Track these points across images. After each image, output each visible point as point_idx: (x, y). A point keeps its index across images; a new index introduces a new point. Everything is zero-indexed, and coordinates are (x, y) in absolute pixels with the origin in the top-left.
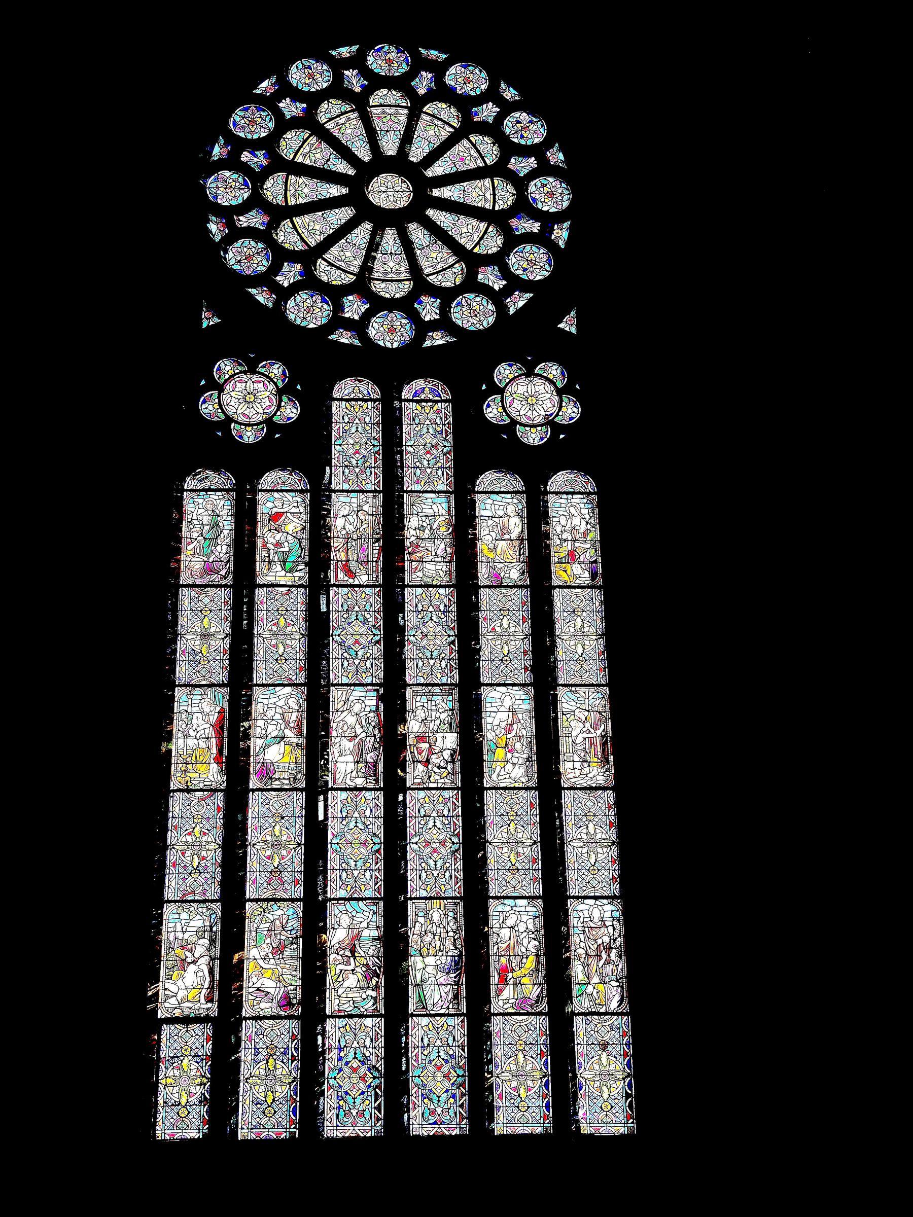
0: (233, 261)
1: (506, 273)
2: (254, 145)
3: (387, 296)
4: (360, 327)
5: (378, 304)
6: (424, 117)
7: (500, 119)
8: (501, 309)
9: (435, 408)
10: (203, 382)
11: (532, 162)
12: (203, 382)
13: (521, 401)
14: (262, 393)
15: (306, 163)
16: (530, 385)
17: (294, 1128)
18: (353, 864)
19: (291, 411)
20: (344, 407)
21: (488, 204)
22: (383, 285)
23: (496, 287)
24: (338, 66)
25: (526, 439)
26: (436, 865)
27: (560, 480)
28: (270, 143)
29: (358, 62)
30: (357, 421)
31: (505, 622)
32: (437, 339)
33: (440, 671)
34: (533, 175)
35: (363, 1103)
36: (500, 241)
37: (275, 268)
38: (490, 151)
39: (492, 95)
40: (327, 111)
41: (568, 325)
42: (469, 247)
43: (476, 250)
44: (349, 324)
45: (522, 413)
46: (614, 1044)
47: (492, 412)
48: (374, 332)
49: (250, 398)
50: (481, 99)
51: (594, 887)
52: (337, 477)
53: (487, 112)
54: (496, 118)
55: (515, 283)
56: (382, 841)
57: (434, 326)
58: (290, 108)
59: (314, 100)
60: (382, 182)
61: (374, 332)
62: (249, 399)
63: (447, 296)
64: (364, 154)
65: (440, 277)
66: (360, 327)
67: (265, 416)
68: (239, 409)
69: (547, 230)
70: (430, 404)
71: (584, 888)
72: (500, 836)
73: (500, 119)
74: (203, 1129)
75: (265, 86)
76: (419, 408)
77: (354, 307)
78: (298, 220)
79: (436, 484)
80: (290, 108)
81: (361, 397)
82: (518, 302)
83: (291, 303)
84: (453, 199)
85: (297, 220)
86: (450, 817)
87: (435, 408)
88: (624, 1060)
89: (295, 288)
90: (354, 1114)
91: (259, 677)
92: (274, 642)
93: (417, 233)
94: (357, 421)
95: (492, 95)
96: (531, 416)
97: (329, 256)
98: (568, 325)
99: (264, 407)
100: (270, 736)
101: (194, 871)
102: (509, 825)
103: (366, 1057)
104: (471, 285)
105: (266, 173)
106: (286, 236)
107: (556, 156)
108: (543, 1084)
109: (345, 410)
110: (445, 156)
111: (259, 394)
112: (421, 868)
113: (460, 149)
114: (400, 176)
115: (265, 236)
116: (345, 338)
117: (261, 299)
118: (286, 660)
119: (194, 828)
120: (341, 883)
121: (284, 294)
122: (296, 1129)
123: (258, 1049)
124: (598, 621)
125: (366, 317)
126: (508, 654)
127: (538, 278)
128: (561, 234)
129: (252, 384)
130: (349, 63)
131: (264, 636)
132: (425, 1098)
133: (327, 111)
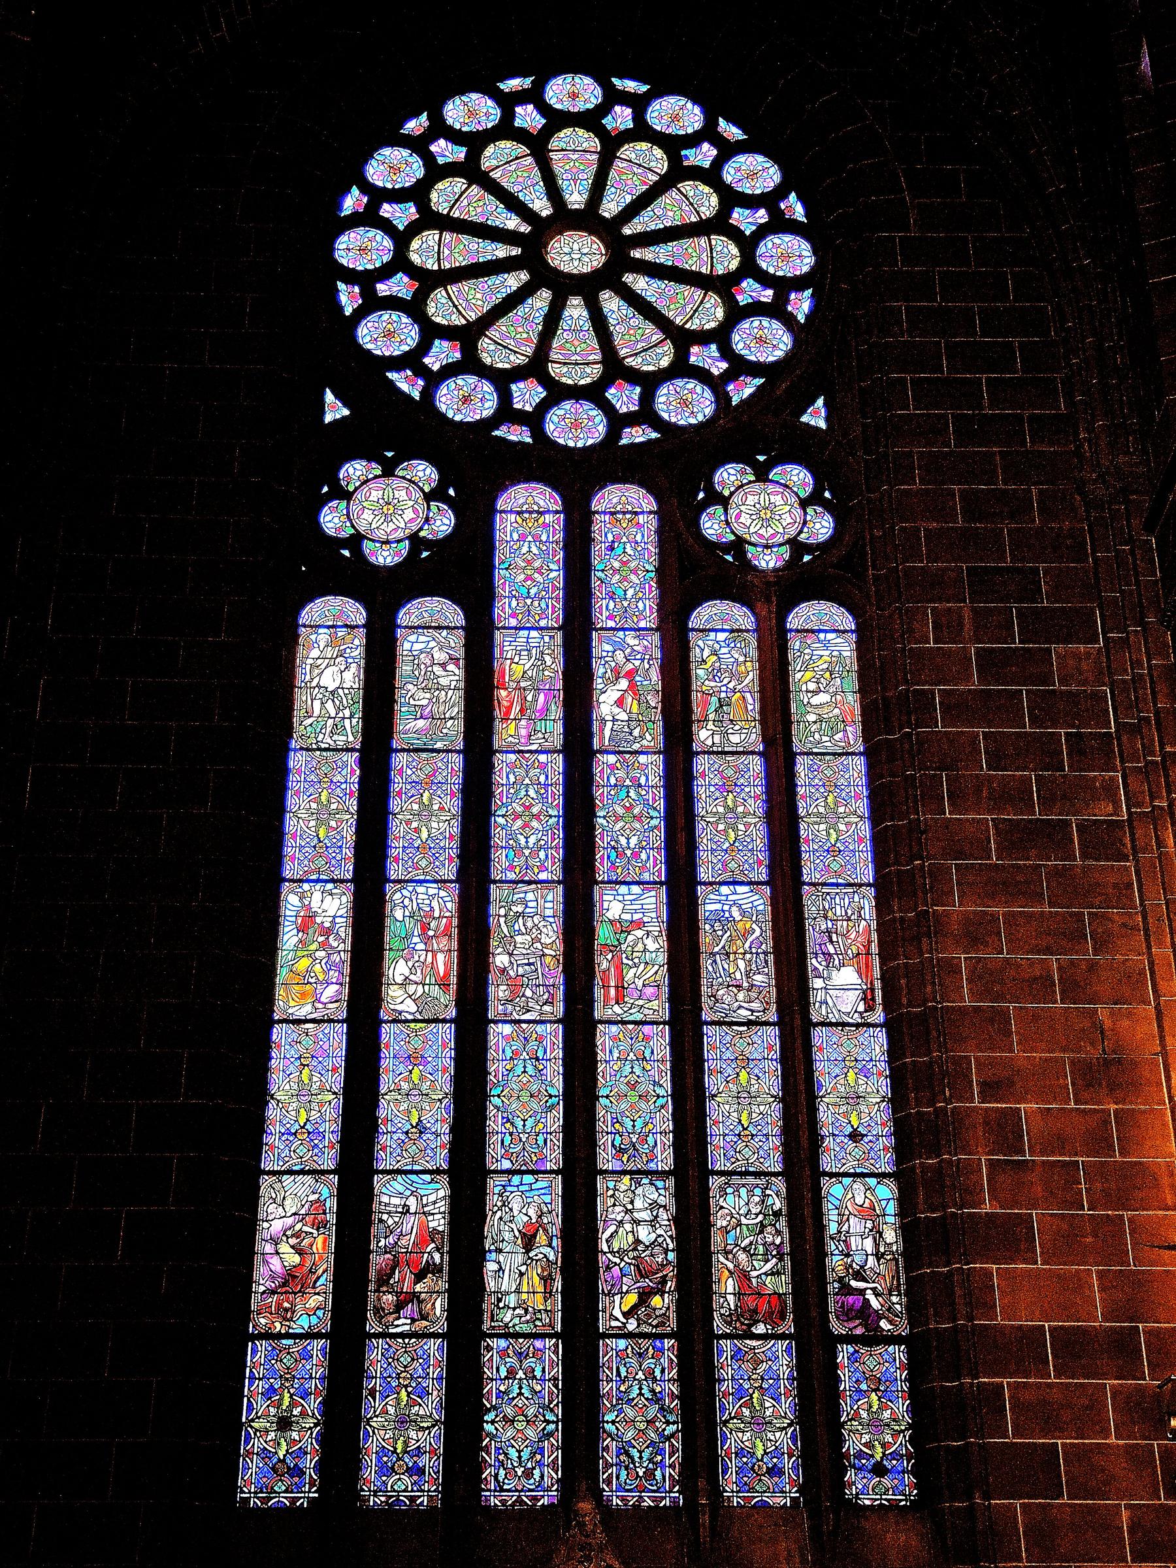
0: (368, 339)
1: (727, 352)
2: (397, 196)
3: (570, 382)
4: (535, 420)
5: (557, 393)
6: (619, 164)
7: (719, 163)
8: (722, 398)
9: (541, 521)
10: (325, 489)
11: (762, 216)
12: (325, 489)
13: (751, 515)
14: (781, 507)
15: (455, 216)
16: (762, 495)
17: (435, 1491)
18: (519, 1124)
19: (443, 523)
20: (513, 520)
21: (705, 267)
22: (565, 369)
23: (716, 372)
24: (508, 103)
25: (374, 558)
26: (634, 1126)
27: (804, 615)
28: (418, 193)
29: (535, 96)
30: (529, 538)
31: (830, 799)
32: (636, 435)
33: (538, 864)
34: (762, 232)
35: (532, 1458)
36: (720, 313)
37: (424, 347)
38: (708, 203)
39: (708, 133)
40: (494, 156)
41: (816, 417)
42: (678, 321)
43: (687, 326)
44: (520, 418)
45: (752, 530)
46: (302, 1378)
47: (712, 526)
48: (552, 427)
49: (766, 513)
50: (693, 140)
51: (301, 1158)
52: (504, 609)
53: (704, 155)
54: (713, 163)
55: (739, 367)
56: (669, 1093)
57: (632, 419)
58: (445, 151)
59: (476, 142)
60: (566, 242)
61: (552, 427)
62: (388, 509)
63: (650, 383)
64: (542, 206)
65: (640, 360)
66: (535, 420)
67: (407, 531)
68: (374, 523)
69: (781, 299)
70: (628, 516)
71: (399, 1158)
72: (287, 1087)
73: (719, 163)
74: (737, 1497)
75: (415, 125)
76: (519, 519)
77: (624, 398)
78: (454, 289)
79: (635, 621)
80: (445, 151)
81: (630, 509)
82: (743, 390)
83: (443, 390)
84: (657, 261)
85: (453, 289)
86: (547, 1060)
87: (541, 521)
88: (903, 1405)
89: (450, 371)
90: (520, 1473)
91: (394, 871)
92: (415, 825)
93: (611, 304)
94: (529, 538)
95: (708, 133)
96: (765, 534)
97: (493, 333)
98: (816, 417)
99: (784, 524)
100: (413, 946)
101: (412, 1130)
102: (738, 1074)
103: (536, 1393)
104: (681, 368)
105: (414, 229)
106: (440, 308)
107: (795, 208)
108: (789, 1436)
109: (608, 526)
110: (649, 209)
111: (777, 508)
112: (504, 1131)
113: (668, 201)
114: (590, 235)
115: (415, 308)
116: (517, 434)
117: (404, 387)
118: (327, 847)
119: (411, 1072)
120: (614, 1152)
121: (434, 380)
122: (439, 1492)
123: (385, 1378)
124: (703, 796)
125: (544, 407)
126: (734, 842)
127: (771, 359)
128: (348, 298)
129: (767, 497)
130: (521, 97)
131: (707, 820)
132: (499, 1454)
133: (494, 156)
